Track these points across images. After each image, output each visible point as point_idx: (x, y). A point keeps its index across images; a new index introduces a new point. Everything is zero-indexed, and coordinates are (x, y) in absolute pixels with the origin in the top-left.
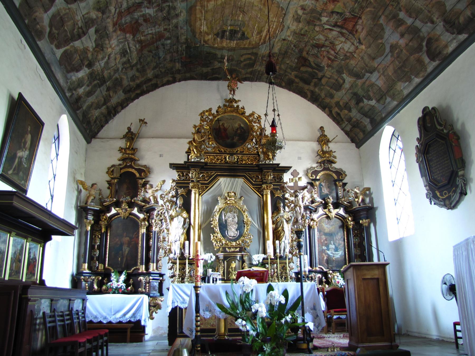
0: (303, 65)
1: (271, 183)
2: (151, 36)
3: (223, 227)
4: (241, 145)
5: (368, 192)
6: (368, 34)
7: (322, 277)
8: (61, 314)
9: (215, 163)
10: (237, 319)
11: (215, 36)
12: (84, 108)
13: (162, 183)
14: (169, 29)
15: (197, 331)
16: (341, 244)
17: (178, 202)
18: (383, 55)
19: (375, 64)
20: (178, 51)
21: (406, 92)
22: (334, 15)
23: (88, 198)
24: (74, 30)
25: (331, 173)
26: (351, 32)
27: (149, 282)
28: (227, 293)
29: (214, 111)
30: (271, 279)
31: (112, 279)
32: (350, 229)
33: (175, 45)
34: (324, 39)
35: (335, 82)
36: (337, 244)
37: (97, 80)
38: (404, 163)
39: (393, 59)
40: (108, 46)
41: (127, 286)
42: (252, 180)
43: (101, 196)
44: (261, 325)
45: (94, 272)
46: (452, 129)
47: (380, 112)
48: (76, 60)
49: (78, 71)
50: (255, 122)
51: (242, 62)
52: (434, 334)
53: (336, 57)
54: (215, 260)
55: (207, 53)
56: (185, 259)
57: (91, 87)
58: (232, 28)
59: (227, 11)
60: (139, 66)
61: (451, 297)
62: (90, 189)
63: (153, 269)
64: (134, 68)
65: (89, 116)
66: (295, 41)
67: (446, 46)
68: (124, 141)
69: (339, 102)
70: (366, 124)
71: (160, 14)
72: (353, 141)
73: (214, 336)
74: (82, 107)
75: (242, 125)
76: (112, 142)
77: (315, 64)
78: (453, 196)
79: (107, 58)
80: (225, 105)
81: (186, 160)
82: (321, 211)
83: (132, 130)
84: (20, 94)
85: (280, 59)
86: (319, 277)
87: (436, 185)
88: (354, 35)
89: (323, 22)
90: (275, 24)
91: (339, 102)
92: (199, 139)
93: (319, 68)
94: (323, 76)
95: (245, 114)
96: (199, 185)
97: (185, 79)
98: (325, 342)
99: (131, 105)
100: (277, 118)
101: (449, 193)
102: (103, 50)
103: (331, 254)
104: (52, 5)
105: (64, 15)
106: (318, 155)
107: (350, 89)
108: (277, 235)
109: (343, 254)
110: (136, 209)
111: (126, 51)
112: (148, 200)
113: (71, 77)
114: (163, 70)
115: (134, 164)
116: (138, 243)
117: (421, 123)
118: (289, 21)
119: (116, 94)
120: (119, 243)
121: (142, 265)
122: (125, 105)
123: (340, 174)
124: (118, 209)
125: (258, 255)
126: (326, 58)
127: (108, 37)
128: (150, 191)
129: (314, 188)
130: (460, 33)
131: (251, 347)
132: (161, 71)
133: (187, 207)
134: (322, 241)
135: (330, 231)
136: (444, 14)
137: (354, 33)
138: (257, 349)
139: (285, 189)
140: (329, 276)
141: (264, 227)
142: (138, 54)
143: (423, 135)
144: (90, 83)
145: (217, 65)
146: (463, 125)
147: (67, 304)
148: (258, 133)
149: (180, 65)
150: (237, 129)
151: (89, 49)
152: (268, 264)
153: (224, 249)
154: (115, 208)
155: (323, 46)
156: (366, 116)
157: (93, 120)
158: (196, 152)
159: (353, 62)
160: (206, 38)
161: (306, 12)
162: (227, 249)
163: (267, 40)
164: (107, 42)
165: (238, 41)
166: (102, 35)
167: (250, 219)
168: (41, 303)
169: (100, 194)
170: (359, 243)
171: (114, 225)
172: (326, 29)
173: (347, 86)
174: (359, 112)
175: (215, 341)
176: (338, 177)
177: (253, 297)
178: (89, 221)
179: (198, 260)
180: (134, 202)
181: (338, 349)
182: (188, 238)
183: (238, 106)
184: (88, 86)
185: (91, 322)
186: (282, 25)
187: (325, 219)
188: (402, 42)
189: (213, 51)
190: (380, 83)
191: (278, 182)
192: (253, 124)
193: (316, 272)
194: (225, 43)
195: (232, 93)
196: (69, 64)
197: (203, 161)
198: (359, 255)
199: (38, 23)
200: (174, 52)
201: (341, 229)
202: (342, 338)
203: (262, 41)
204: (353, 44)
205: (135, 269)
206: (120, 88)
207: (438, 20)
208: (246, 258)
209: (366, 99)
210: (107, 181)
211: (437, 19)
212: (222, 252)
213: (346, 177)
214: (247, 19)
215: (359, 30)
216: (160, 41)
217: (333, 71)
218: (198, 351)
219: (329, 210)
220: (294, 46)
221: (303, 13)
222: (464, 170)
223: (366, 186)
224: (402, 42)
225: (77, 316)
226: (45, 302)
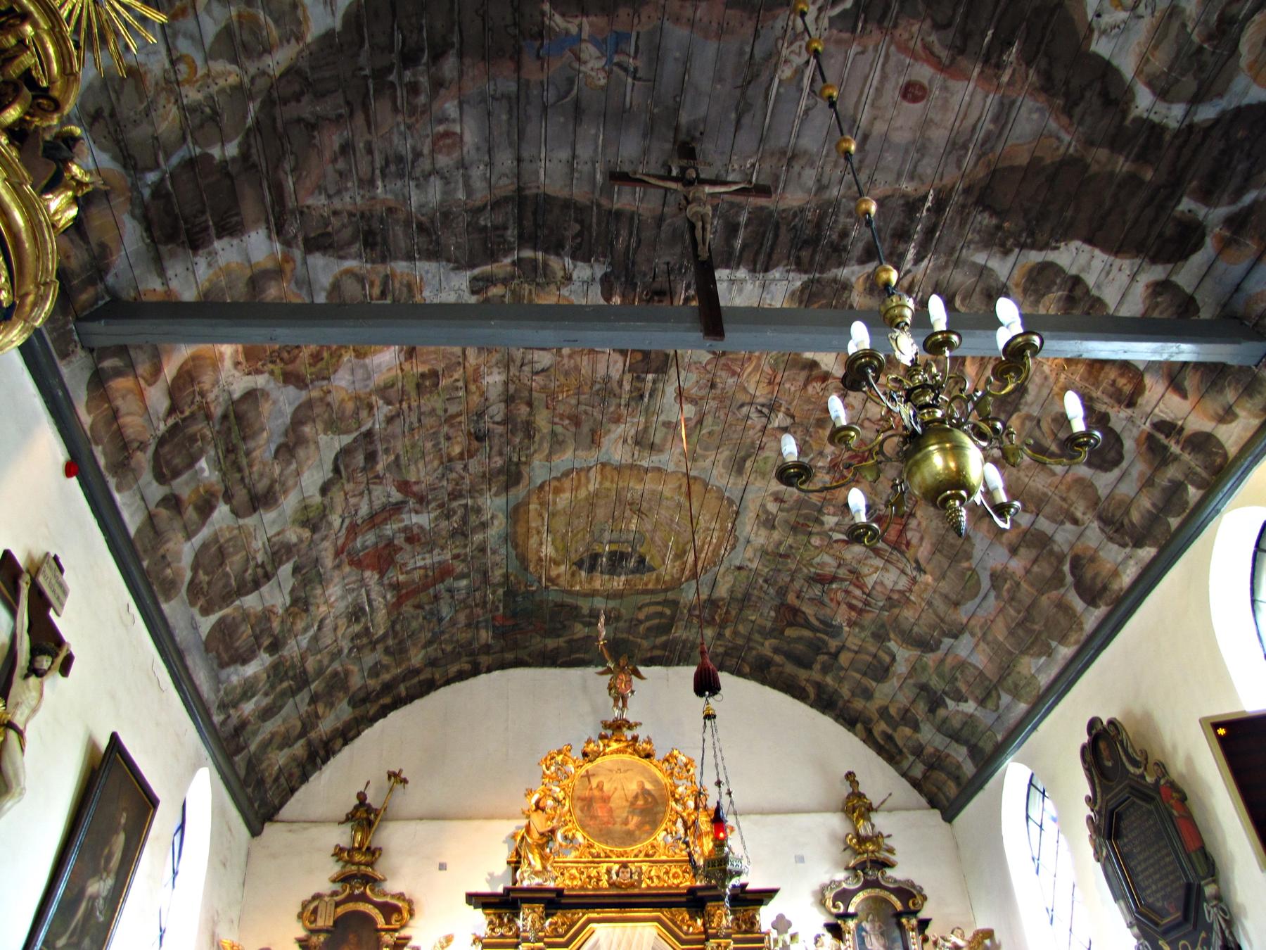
0: (791, 624)
2: (422, 572)
5: (987, 942)
6: (937, 548)
11: (574, 568)
12: (253, 747)
14: (466, 555)
18: (976, 596)
19: (962, 615)
20: (485, 603)
21: (1044, 680)
22: (1113, 96)
24: (246, 570)
25: (884, 894)
26: (896, 546)
33: (478, 589)
34: (834, 563)
35: (870, 659)
37: (290, 679)
39: (1002, 604)
40: (321, 601)
47: (989, 729)
48: (244, 636)
49: (245, 662)
51: (641, 622)
53: (866, 603)
55: (556, 605)
58: (614, 547)
59: (601, 513)
60: (390, 642)
64: (378, 647)
65: (264, 765)
67: (1115, 574)
68: (347, 828)
69: (887, 708)
70: (960, 759)
71: (444, 524)
72: (933, 804)
74: (246, 746)
75: (648, 786)
76: (314, 831)
77: (818, 619)
84: (114, 738)
85: (734, 613)
87: (1157, 924)
88: (903, 553)
89: (827, 527)
90: (716, 534)
91: (887, 708)
93: (831, 629)
97: (503, 666)
99: (367, 733)
100: (725, 801)
102: (307, 610)
104: (203, 524)
105: (228, 541)
106: (847, 847)
111: (362, 609)
113: (229, 676)
114: (449, 648)
115: (372, 890)
117: (1089, 758)
118: (747, 525)
123: (908, 893)
126: (844, 607)
127: (321, 580)
130: (1138, 544)
132: (443, 650)
136: (1096, 504)
137: (904, 547)
142: (389, 613)
143: (1098, 789)
144: (273, 687)
145: (580, 631)
149: (490, 634)
150: (636, 797)
151: (275, 610)
155: (834, 579)
156: (957, 741)
157: (271, 775)
159: (908, 614)
160: (554, 573)
161: (786, 506)
165: (630, 577)
166: (310, 575)
172: (836, 541)
173: (901, 668)
174: (939, 730)
176: (905, 904)
184: (266, 694)
186: (731, 536)
188: (1016, 565)
189: (569, 600)
190: (980, 659)
191: (746, 932)
194: (599, 582)
195: (620, 704)
196: (226, 647)
199: (169, 565)
200: (477, 605)
203: (687, 573)
204: (903, 572)
206: (341, 695)
207: (1086, 517)
209: (952, 699)
211: (1084, 514)
214: (649, 527)
215: (914, 541)
216: (443, 581)
217: (863, 635)
220: (766, 581)
221: (780, 509)
222: (1215, 881)
223: (982, 925)
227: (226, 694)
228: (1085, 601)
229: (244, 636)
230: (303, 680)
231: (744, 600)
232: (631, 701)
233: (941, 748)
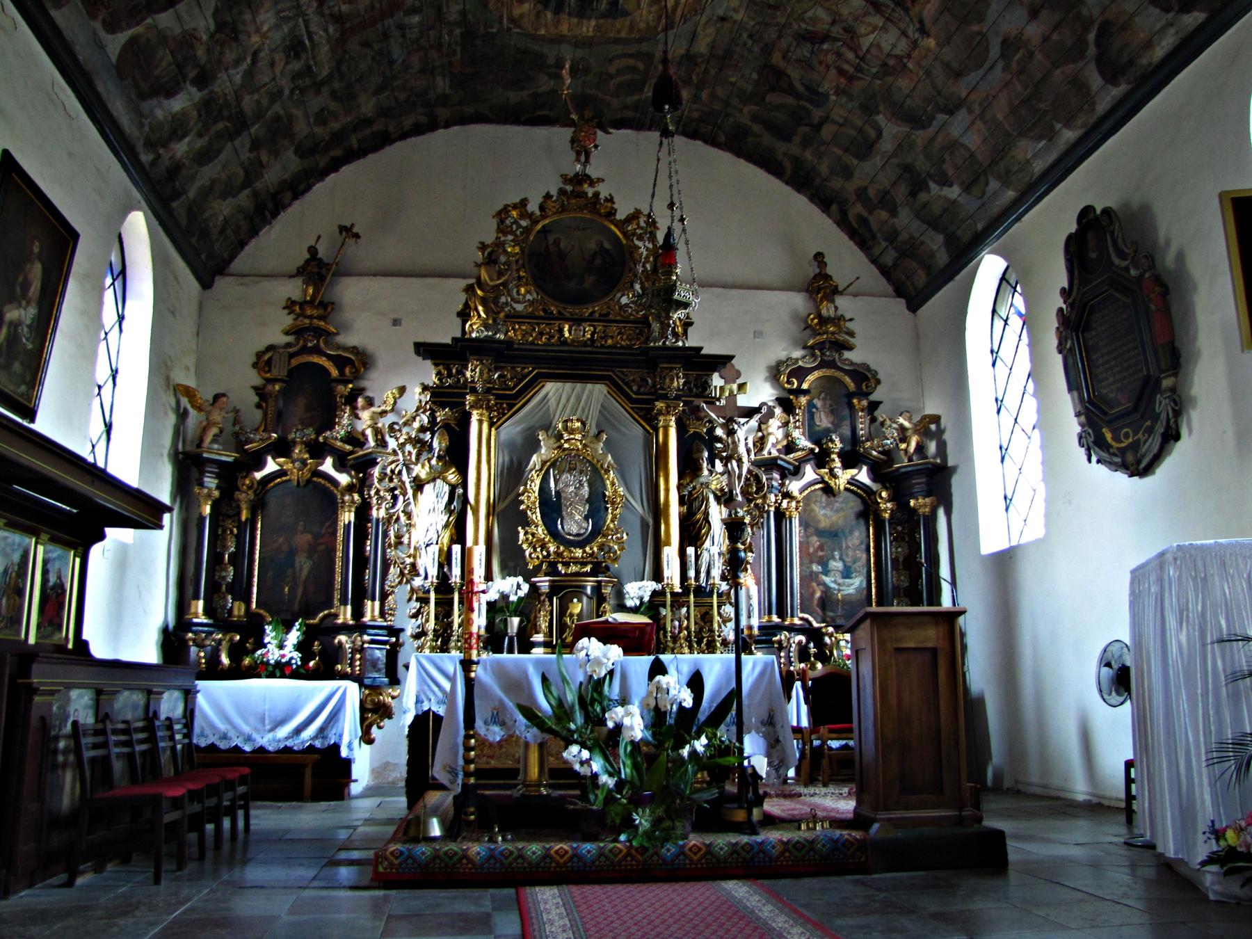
0: (773, 89)
1: (678, 398)
3: (552, 508)
4: (603, 298)
5: (933, 427)
7: (808, 642)
8: (121, 726)
9: (532, 343)
10: (569, 743)
11: (539, 7)
12: (192, 194)
13: (400, 395)
15: (467, 774)
16: (860, 559)
17: (436, 444)
20: (440, 44)
21: (1039, 166)
23: (204, 430)
25: (838, 374)
27: (362, 650)
28: (545, 680)
29: (533, 207)
30: (671, 644)
31: (267, 640)
32: (883, 521)
33: (432, 28)
34: (829, 19)
35: (854, 133)
36: (848, 560)
37: (221, 118)
38: (1027, 349)
40: (251, 28)
41: (305, 660)
42: (631, 388)
43: (237, 428)
44: (628, 762)
45: (219, 619)
46: (1152, 266)
48: (164, 64)
49: (170, 94)
50: (640, 238)
51: (611, 77)
52: (1080, 789)
54: (528, 595)
56: (451, 591)
57: (206, 138)
60: (336, 85)
61: (1121, 699)
62: (209, 408)
63: (373, 616)
65: (207, 214)
66: (752, 23)
67: (1149, 45)
68: (299, 282)
69: (865, 189)
70: (935, 248)
72: (899, 292)
73: (515, 786)
75: (607, 245)
76: (267, 285)
77: (803, 85)
78: (1145, 442)
79: (249, 60)
80: (562, 192)
81: (458, 334)
82: (810, 473)
83: (320, 255)
85: (712, 72)
86: (800, 642)
87: (1105, 413)
88: (906, 10)
91: (865, 189)
92: (492, 280)
93: (817, 98)
94: (826, 119)
95: (615, 214)
96: (489, 401)
97: (463, 121)
98: (798, 806)
100: (677, 226)
101: (1136, 433)
102: (236, 39)
103: (832, 585)
107: (895, 154)
108: (693, 533)
109: (864, 585)
110: (329, 461)
111: (302, 43)
112: (362, 439)
113: (152, 111)
114: (402, 96)
115: (326, 343)
116: (334, 550)
119: (276, 157)
120: (285, 548)
121: (346, 604)
122: (302, 187)
123: (865, 378)
124: (282, 460)
125: (640, 584)
126: (833, 72)
128: (365, 415)
129: (794, 414)
131: (602, 814)
132: (396, 99)
133: (457, 456)
134: (811, 550)
135: (832, 525)
138: (618, 821)
139: (703, 414)
140: (827, 640)
141: (658, 511)
143: (1076, 281)
146: (1180, 256)
147: (142, 703)
148: (648, 267)
149: (447, 81)
150: (595, 254)
152: (665, 607)
153: (553, 565)
154: (274, 459)
155: (826, 37)
158: (483, 315)
159: (903, 84)
160: (517, 12)
162: (560, 567)
163: (677, 19)
164: (248, 17)
165: (601, 21)
167: (621, 490)
168: (69, 699)
169: (236, 421)
170: (905, 559)
171: (273, 502)
173: (887, 145)
174: (917, 215)
175: (516, 799)
176: (858, 386)
177: (613, 690)
178: (206, 491)
179: (472, 592)
180: (325, 443)
181: (826, 825)
182: (459, 535)
183: (597, 195)
184: (200, 135)
185: (212, 747)
187: (820, 493)
192: (637, 242)
193: (792, 629)
195: (583, 158)
196: (145, 72)
197: (502, 337)
198: (906, 589)
200: (431, 47)
201: (862, 522)
202: (845, 798)
204: (904, 33)
205: (325, 617)
206: (286, 142)
208: (607, 591)
209: (935, 182)
210: (256, 388)
212: (546, 575)
213: (879, 387)
216: (392, 15)
217: (850, 106)
218: (470, 823)
219: (831, 470)
220: (750, 36)
222: (1176, 375)
223: (929, 410)
224: (1034, 31)
225: (168, 733)
226: (81, 696)
227: (152, 129)
228: (1103, 78)
229: (164, 64)
230: (240, 123)
231: (724, 57)
232: (595, 154)
233: (916, 235)
